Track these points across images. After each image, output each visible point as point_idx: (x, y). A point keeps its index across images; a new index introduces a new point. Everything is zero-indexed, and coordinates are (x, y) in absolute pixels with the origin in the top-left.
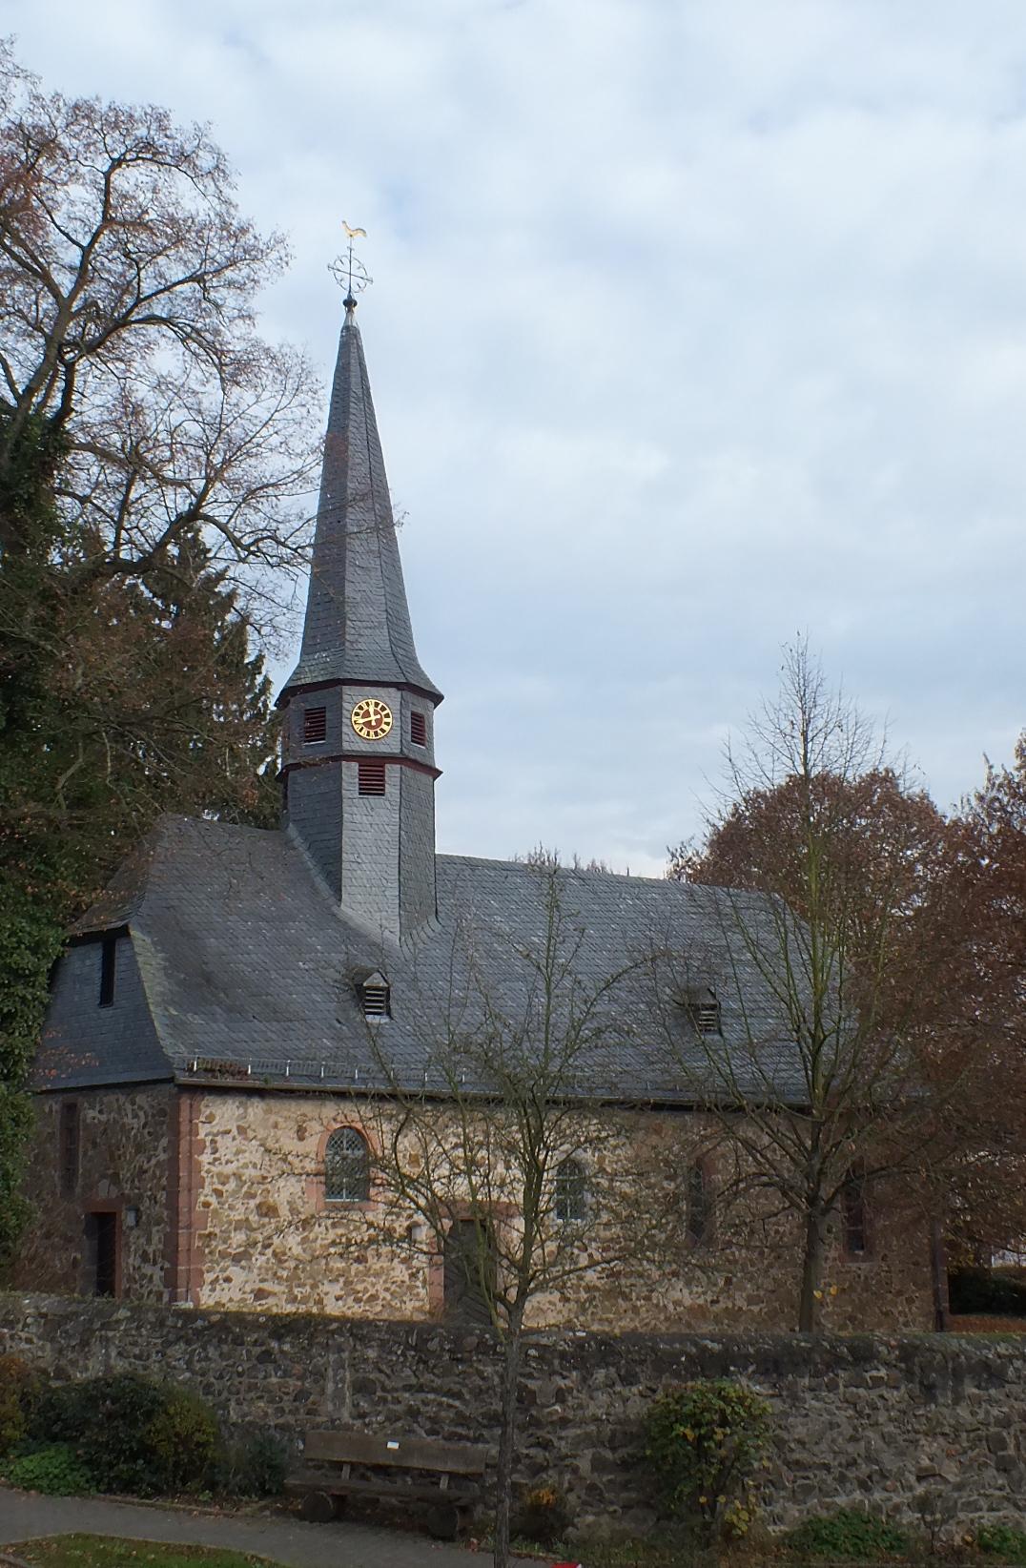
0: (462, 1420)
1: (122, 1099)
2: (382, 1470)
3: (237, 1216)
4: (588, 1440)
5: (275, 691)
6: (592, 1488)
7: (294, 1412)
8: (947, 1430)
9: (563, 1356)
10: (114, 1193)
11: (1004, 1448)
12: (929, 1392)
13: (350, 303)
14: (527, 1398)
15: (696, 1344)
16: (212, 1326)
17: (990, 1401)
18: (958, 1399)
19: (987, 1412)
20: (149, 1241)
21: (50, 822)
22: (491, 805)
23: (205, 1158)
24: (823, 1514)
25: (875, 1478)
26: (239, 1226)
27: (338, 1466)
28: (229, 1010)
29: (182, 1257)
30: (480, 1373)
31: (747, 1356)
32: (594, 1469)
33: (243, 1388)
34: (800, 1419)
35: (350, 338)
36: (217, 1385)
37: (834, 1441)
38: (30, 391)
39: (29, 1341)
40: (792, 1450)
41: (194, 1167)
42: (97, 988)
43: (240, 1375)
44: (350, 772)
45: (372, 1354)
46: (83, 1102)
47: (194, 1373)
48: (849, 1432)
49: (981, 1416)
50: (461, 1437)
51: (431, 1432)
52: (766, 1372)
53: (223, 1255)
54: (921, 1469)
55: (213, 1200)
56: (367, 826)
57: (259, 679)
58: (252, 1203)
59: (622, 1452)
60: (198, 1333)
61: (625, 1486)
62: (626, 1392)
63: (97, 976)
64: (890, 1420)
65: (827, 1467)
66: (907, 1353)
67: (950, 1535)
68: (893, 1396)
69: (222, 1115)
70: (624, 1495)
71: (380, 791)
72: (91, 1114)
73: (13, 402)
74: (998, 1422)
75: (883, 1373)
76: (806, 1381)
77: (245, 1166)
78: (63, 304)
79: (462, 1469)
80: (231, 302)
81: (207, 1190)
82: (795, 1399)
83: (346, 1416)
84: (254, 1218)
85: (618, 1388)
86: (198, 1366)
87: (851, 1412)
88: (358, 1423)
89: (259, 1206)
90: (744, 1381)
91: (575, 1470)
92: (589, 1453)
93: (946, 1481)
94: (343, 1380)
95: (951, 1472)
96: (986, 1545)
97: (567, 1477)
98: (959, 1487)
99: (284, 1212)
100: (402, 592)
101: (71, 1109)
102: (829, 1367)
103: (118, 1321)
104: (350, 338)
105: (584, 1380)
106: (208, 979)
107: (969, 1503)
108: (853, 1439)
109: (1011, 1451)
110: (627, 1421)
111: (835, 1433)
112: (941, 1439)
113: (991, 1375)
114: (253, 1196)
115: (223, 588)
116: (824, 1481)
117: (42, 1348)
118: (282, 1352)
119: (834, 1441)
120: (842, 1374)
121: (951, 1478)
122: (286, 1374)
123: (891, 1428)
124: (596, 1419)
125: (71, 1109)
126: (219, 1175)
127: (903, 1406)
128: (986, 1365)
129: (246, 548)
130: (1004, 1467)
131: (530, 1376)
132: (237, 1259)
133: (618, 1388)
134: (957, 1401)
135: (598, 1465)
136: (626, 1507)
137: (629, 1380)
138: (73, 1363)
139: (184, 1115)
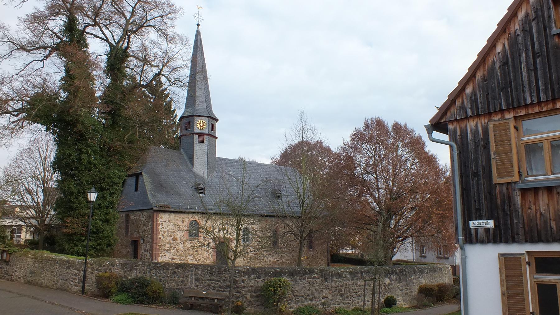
0: (220, 287)
1: (140, 213)
2: (202, 298)
3: (167, 241)
4: (249, 291)
5: (178, 118)
6: (250, 301)
9: (244, 272)
10: (138, 236)
12: (326, 280)
13: (198, 25)
14: (235, 282)
16: (162, 266)
20: (146, 246)
21: (123, 147)
22: (230, 145)
23: (160, 227)
24: (302, 306)
26: (168, 243)
27: (191, 297)
28: (166, 193)
29: (154, 250)
31: (286, 272)
35: (198, 34)
36: (163, 279)
38: (119, 42)
39: (117, 269)
42: (134, 187)
44: (196, 137)
45: (199, 272)
46: (130, 214)
48: (308, 289)
50: (220, 291)
52: (290, 276)
53: (164, 250)
55: (162, 237)
56: (200, 150)
57: (175, 114)
58: (171, 238)
59: (257, 294)
61: (257, 301)
63: (134, 184)
65: (303, 296)
66: (321, 271)
68: (318, 281)
69: (164, 217)
71: (203, 142)
72: (132, 217)
73: (115, 44)
74: (341, 286)
75: (316, 275)
78: (128, 21)
79: (220, 298)
80: (169, 23)
81: (161, 235)
82: (296, 282)
83: (193, 286)
84: (171, 241)
91: (246, 298)
92: (249, 294)
95: (330, 297)
98: (332, 300)
99: (179, 240)
100: (209, 95)
101: (127, 216)
102: (304, 274)
104: (198, 34)
106: (161, 185)
108: (309, 290)
109: (343, 292)
110: (258, 287)
115: (166, 92)
122: (179, 277)
123: (317, 288)
124: (251, 286)
125: (127, 216)
128: (338, 273)
129: (172, 83)
132: (167, 251)
134: (332, 282)
135: (252, 296)
138: (128, 274)
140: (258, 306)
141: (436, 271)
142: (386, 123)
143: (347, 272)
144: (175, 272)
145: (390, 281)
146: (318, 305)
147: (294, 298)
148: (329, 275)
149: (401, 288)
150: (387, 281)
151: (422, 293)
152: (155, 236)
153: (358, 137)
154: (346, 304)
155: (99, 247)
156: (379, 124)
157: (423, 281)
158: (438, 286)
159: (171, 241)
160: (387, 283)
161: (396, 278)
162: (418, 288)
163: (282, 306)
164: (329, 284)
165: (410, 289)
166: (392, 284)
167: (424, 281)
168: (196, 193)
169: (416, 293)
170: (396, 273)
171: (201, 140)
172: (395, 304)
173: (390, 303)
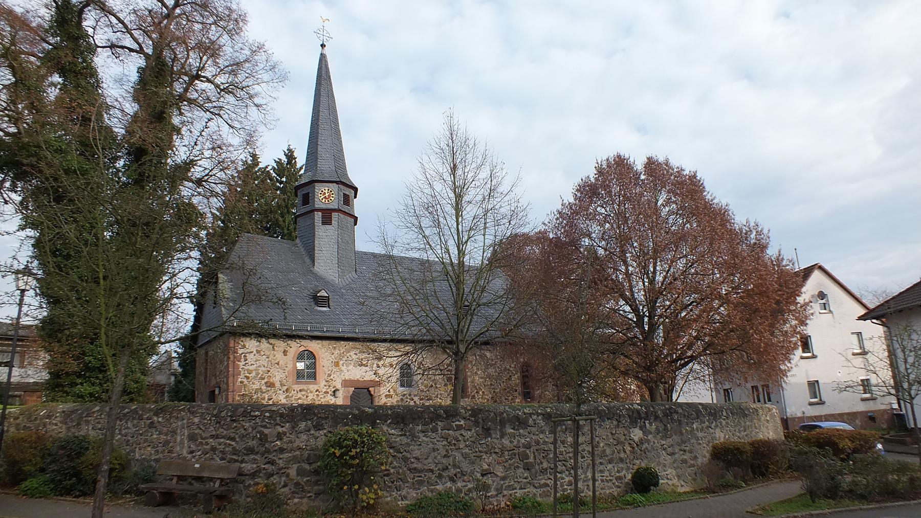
0: (235, 452)
3: (255, 387)
4: (295, 459)
6: (297, 484)
7: (163, 452)
8: (497, 450)
9: (282, 415)
11: (528, 459)
12: (487, 432)
13: (323, 46)
14: (264, 439)
15: (359, 409)
17: (520, 435)
18: (503, 436)
19: (519, 441)
23: (241, 364)
24: (430, 495)
25: (459, 475)
30: (243, 426)
31: (387, 415)
32: (298, 475)
33: (142, 441)
34: (416, 447)
35: (323, 58)
37: (435, 458)
39: (56, 425)
40: (412, 463)
41: (236, 367)
43: (141, 435)
44: (318, 216)
47: (122, 435)
49: (515, 443)
50: (236, 461)
51: (222, 459)
52: (397, 423)
54: (483, 470)
55: (245, 380)
56: (325, 237)
58: (263, 382)
59: (315, 466)
60: (125, 415)
61: (316, 483)
62: (317, 434)
64: (466, 446)
65: (432, 471)
67: (499, 502)
69: (251, 344)
70: (316, 487)
74: (524, 446)
75: (462, 422)
76: (420, 428)
77: (260, 366)
81: (242, 376)
82: (413, 437)
83: (185, 452)
84: (264, 388)
85: (312, 432)
86: (123, 432)
87: (445, 443)
88: (190, 456)
89: (266, 383)
90: (385, 428)
91: (288, 476)
92: (295, 466)
93: (497, 476)
94: (184, 435)
95: (500, 471)
96: (516, 506)
97: (283, 479)
98: (504, 478)
99: (278, 385)
100: (342, 150)
102: (432, 420)
103: (94, 413)
104: (323, 58)
105: (293, 428)
107: (509, 486)
108: (445, 456)
109: (531, 460)
110: (317, 449)
111: (436, 454)
112: (494, 455)
113: (520, 423)
114: (264, 379)
116: (430, 478)
117: (61, 428)
118: (159, 422)
119: (435, 458)
120: (439, 423)
121: (499, 474)
122: (160, 433)
123: (467, 450)
124: (300, 449)
126: (248, 370)
127: (473, 439)
128: (517, 418)
130: (527, 468)
131: (265, 427)
133: (312, 432)
134: (502, 436)
135: (300, 472)
136: (318, 494)
137: (318, 427)
139: (232, 345)
140: (318, 494)
141: (746, 415)
142: (632, 160)
143: (538, 414)
144: (152, 423)
145: (644, 433)
146: (470, 490)
147: (410, 476)
148: (494, 421)
149: (670, 450)
150: (637, 434)
151: (718, 459)
152: (231, 379)
153: (589, 192)
154: (541, 486)
155: (104, 396)
156: (620, 165)
157: (721, 436)
158: (752, 444)
159: (264, 388)
160: (636, 439)
161: (657, 428)
162: (710, 448)
163: (367, 495)
164: (494, 440)
165: (691, 452)
166: (648, 442)
167: (722, 435)
168: (312, 304)
169: (706, 460)
170: (657, 418)
171: (327, 221)
172: (656, 484)
173: (644, 482)
